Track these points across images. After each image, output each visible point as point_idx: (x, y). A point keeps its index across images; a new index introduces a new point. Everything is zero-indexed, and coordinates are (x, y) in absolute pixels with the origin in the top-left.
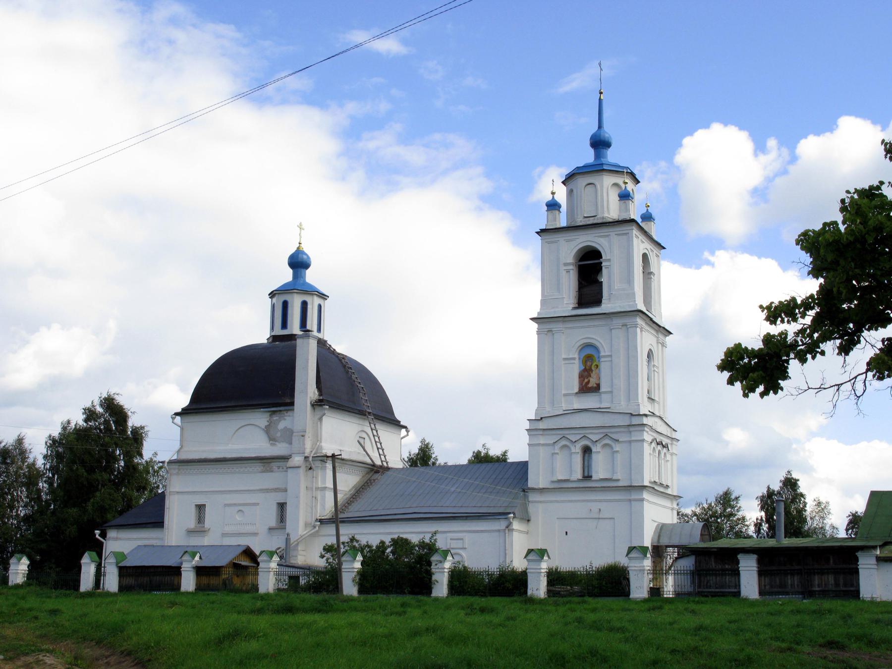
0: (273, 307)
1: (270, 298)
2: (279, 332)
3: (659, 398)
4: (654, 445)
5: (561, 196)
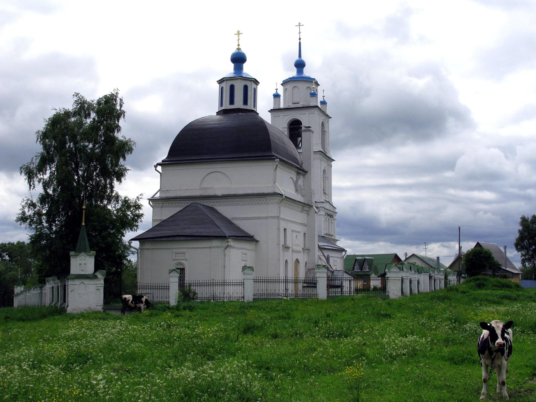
0: (222, 90)
1: (218, 83)
2: (227, 106)
3: (328, 192)
4: (326, 216)
5: (281, 92)
